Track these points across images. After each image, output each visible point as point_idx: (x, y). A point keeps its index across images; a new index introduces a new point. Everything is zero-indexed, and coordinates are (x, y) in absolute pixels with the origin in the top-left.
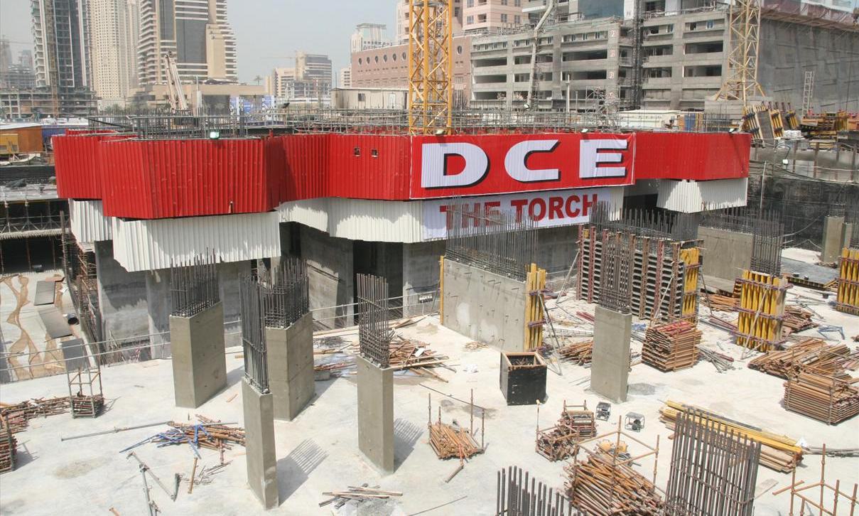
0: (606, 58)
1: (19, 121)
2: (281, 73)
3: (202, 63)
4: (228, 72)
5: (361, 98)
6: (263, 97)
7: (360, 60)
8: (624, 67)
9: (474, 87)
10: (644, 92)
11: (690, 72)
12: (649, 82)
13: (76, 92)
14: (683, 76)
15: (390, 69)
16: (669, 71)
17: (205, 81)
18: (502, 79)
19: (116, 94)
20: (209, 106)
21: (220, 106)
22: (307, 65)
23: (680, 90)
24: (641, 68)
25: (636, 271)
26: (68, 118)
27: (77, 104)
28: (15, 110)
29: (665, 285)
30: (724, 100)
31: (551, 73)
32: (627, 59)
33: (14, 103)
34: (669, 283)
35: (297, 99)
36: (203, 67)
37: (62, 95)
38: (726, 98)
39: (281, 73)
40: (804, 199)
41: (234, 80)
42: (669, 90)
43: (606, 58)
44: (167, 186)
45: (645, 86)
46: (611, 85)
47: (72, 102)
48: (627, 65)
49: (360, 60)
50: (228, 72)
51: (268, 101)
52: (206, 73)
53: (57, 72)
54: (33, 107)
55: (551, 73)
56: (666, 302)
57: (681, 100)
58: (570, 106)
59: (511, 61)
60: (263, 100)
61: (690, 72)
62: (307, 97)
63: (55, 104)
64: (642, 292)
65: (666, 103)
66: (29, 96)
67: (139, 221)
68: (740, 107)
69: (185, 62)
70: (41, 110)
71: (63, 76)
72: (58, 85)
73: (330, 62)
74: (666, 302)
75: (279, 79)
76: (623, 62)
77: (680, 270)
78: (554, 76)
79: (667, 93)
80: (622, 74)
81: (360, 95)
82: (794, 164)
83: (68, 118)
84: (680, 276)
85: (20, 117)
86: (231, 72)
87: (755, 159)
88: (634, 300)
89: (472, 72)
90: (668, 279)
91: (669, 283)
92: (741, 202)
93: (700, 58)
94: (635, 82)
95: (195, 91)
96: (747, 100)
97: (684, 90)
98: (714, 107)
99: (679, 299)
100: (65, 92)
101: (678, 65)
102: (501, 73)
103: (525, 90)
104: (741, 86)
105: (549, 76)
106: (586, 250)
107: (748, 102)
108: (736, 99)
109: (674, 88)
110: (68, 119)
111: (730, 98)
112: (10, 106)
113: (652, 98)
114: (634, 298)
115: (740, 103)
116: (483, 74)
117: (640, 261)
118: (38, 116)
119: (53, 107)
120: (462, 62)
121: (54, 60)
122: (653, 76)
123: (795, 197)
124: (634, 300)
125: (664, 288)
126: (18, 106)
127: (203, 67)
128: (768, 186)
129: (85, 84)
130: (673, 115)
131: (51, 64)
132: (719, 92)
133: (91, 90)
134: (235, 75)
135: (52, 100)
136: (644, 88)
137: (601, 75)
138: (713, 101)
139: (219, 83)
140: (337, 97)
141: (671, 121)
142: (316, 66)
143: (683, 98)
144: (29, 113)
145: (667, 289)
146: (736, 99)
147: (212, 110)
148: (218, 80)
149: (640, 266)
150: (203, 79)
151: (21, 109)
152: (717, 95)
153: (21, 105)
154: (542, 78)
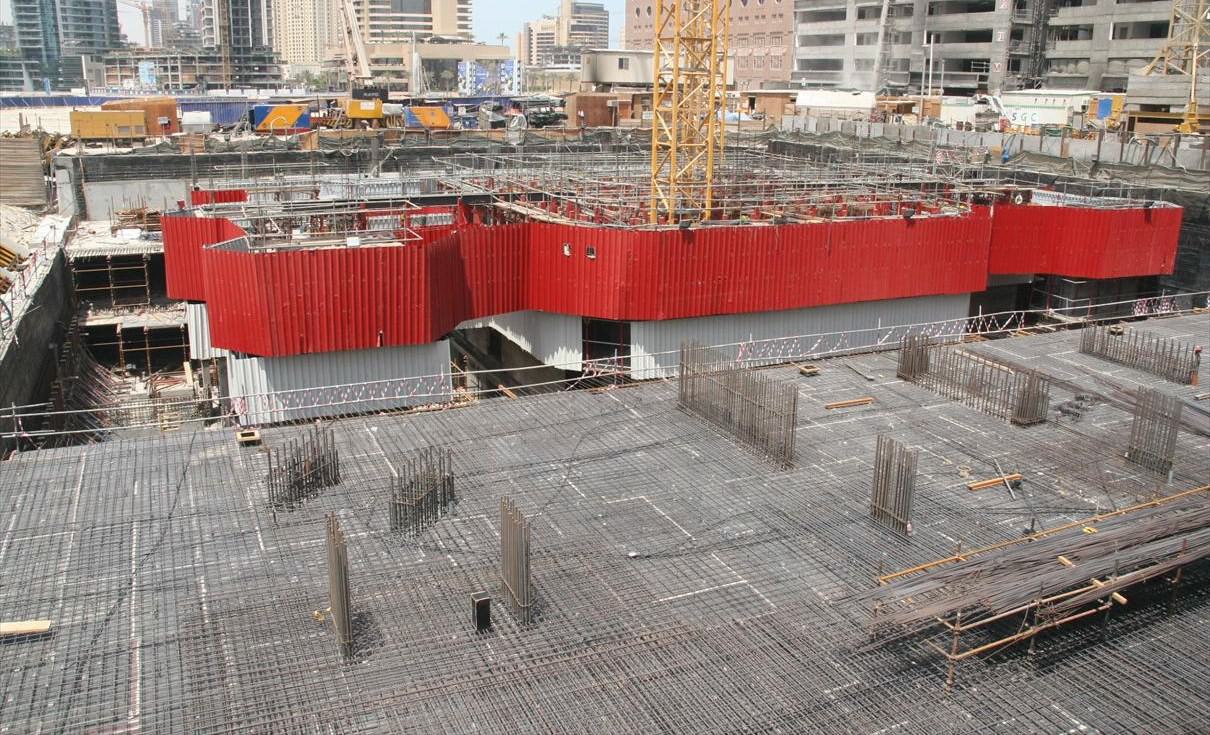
0: (993, 10)
1: (179, 92)
2: (537, 30)
3: (964, 71)
4: (461, 27)
5: (622, 64)
6: (502, 62)
7: (638, 11)
8: (1020, 24)
9: (798, 51)
10: (1048, 63)
11: (1121, 32)
12: (1057, 47)
13: (253, 54)
14: (1111, 38)
15: (643, 27)
16: (1089, 31)
17: (429, 39)
18: (839, 39)
19: (310, 57)
20: (432, 74)
21: (447, 74)
22: (574, 18)
23: (1105, 60)
24: (1046, 26)
26: (242, 89)
27: (254, 71)
28: (175, 78)
30: (1160, 75)
31: (910, 33)
32: (1025, 12)
33: (174, 69)
35: (558, 66)
36: (426, 20)
37: (236, 58)
38: (1165, 71)
39: (537, 30)
41: (469, 39)
42: (1088, 59)
43: (993, 10)
44: (291, 313)
45: (1050, 54)
46: (997, 52)
47: (248, 68)
48: (1025, 22)
49: (638, 11)
50: (461, 27)
51: (508, 68)
52: (431, 28)
53: (229, 27)
54: (198, 73)
55: (910, 33)
57: (1104, 75)
58: (932, 82)
59: (852, 14)
60: (503, 66)
61: (1121, 32)
62: (572, 63)
63: (226, 70)
65: (1080, 82)
66: (193, 59)
67: (255, 359)
68: (1184, 86)
69: (402, 11)
70: (208, 78)
71: (237, 32)
72: (230, 45)
73: (607, 13)
75: (534, 37)
76: (1019, 17)
78: (914, 38)
79: (1082, 65)
80: (1016, 34)
81: (621, 60)
83: (242, 89)
85: (181, 88)
86: (465, 27)
87: (1202, 167)
89: (796, 30)
93: (1139, 9)
94: (1036, 47)
95: (410, 53)
96: (1197, 75)
97: (1110, 59)
98: (1142, 86)
100: (238, 53)
101: (1102, 22)
102: (837, 32)
103: (870, 57)
104: (1190, 53)
105: (906, 38)
107: (1199, 77)
108: (1181, 73)
109: (1096, 56)
110: (242, 91)
111: (1170, 71)
112: (169, 73)
113: (1060, 71)
115: (1187, 79)
116: (811, 33)
118: (205, 86)
119: (224, 74)
120: (781, 15)
121: (225, 10)
122: (1064, 38)
126: (179, 73)
127: (426, 20)
129: (265, 42)
130: (1087, 98)
131: (222, 15)
132: (1152, 64)
133: (274, 50)
134: (468, 31)
135: (222, 64)
136: (1048, 56)
137: (985, 36)
138: (1141, 76)
139: (447, 41)
140: (588, 62)
141: (1084, 107)
142: (588, 18)
143: (1107, 73)
144: (194, 82)
146: (1181, 73)
147: (437, 83)
148: (446, 37)
150: (426, 35)
151: (184, 78)
152: (1149, 67)
153: (182, 71)
154: (896, 40)
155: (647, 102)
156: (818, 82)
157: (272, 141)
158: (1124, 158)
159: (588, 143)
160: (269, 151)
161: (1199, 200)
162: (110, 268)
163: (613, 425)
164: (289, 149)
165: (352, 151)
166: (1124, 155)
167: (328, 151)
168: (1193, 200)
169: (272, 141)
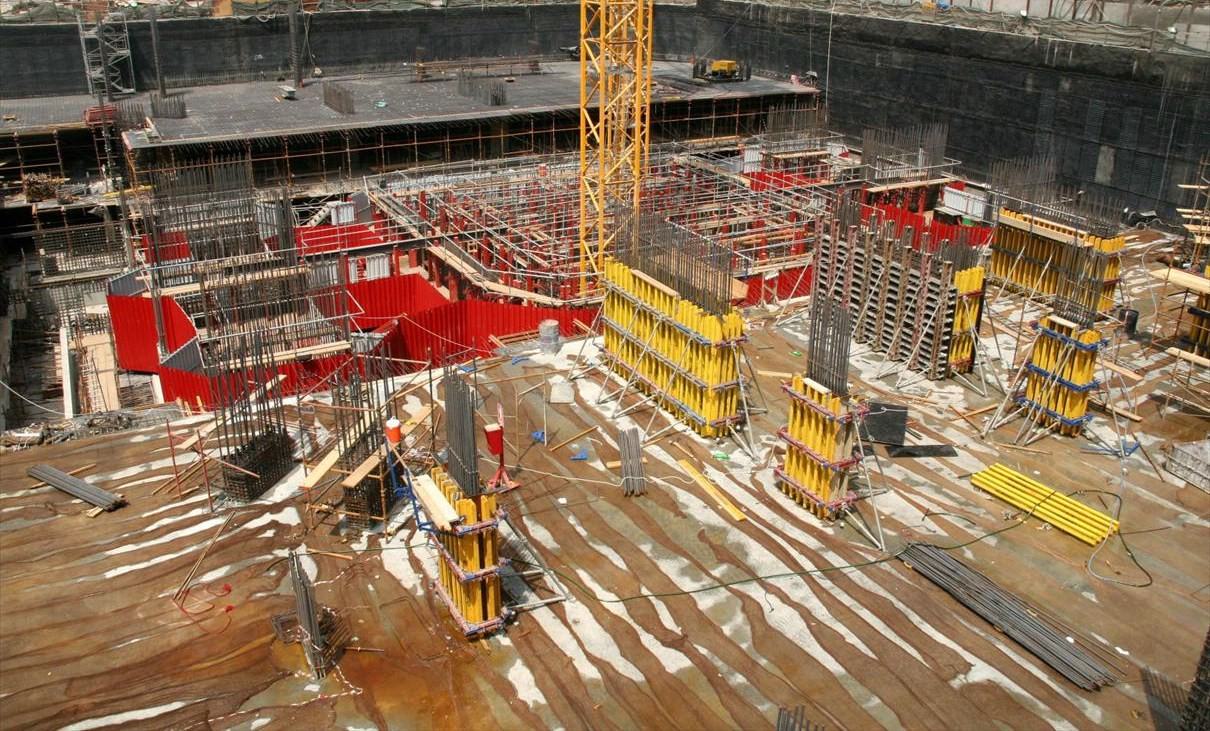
25: (890, 291)
29: (928, 317)
34: (933, 315)
40: (1194, 88)
56: (927, 340)
64: (900, 305)
74: (927, 340)
77: (950, 299)
82: (1188, 30)
84: (950, 307)
88: (886, 332)
90: (933, 309)
91: (933, 315)
92: (899, 479)
99: (948, 340)
106: (824, 251)
114: (885, 328)
117: (897, 277)
123: (1181, 82)
124: (886, 332)
125: (926, 321)
128: (1141, 65)
145: (930, 322)
149: (896, 285)
155: (344, 412)
156: (305, 175)
157: (182, 7)
158: (1052, 14)
159: (338, 647)
160: (181, 19)
161: (1125, 56)
162: (18, 146)
163: (900, 357)
164: (202, 15)
165: (269, 17)
166: (1053, 10)
167: (242, 17)
168: (1118, 55)
169: (182, 7)
